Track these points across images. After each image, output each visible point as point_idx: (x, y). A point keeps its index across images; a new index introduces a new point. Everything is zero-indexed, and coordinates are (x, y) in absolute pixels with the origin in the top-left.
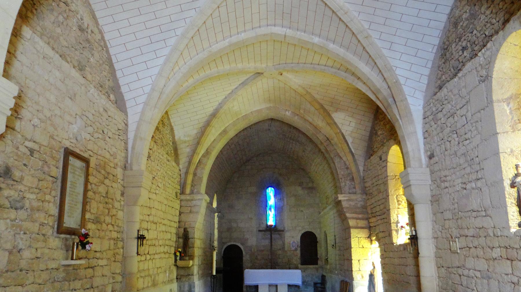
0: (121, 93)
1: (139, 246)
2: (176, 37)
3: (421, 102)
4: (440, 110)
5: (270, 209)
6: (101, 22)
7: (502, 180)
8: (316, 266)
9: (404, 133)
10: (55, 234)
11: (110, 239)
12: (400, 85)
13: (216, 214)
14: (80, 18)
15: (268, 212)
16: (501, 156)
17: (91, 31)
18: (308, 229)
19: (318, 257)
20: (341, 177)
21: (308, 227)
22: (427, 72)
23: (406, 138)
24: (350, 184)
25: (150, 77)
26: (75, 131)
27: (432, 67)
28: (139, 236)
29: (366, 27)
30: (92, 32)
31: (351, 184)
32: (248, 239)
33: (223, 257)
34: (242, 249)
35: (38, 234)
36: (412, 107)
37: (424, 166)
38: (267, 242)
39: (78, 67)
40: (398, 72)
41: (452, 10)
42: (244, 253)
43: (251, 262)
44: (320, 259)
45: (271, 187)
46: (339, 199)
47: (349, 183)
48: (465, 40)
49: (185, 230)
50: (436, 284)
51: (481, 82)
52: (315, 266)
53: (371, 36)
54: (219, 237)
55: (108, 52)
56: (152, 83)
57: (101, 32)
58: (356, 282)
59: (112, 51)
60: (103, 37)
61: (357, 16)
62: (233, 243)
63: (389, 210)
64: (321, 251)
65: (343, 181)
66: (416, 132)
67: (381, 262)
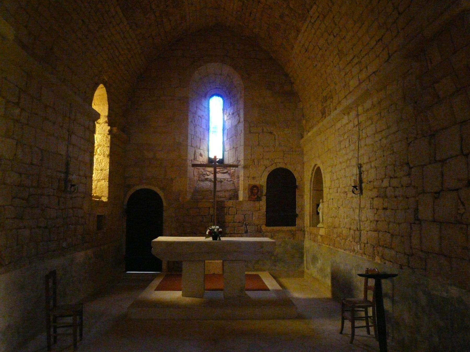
8: (293, 228)
21: (281, 161)
34: (163, 197)
42: (165, 204)
45: (218, 95)
52: (289, 228)
67: (260, 237)
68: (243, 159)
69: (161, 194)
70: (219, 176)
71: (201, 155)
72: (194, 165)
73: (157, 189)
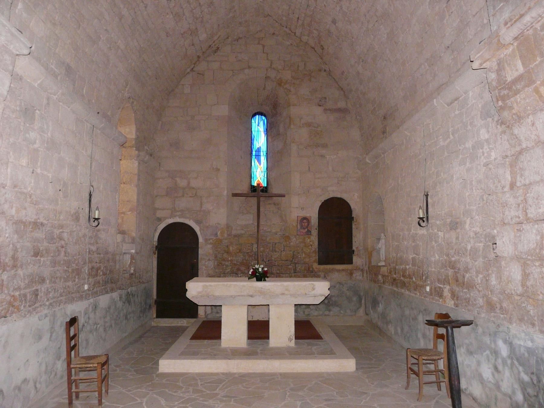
5: (258, 156)
15: (254, 162)
18: (334, 192)
19: (354, 248)
32: (209, 212)
38: (249, 219)
42: (201, 240)
43: (216, 257)
44: (356, 253)
62: (178, 220)
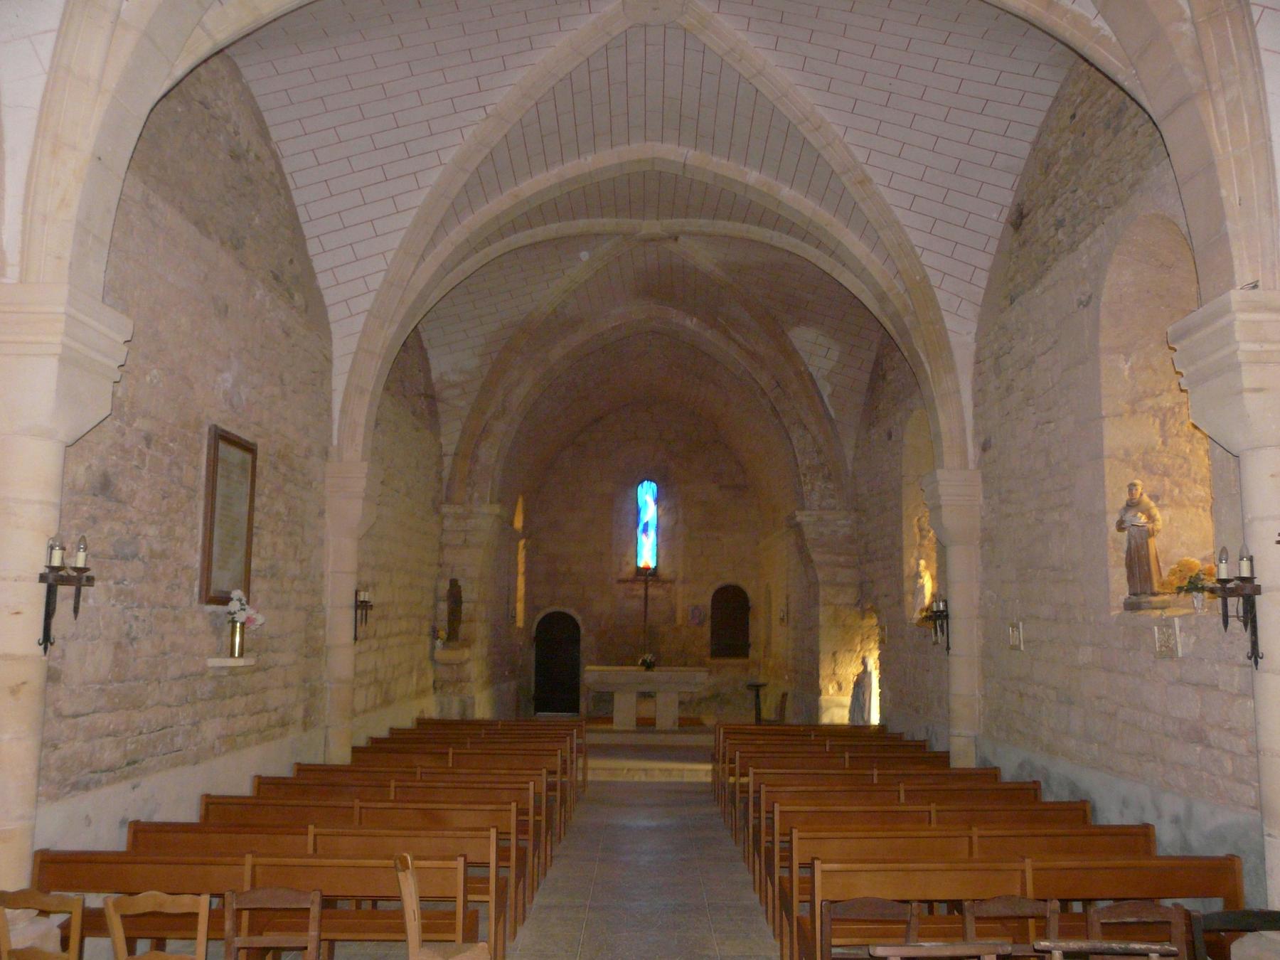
0: (318, 290)
1: (359, 624)
2: (441, 168)
3: (973, 327)
4: (1008, 351)
5: (645, 530)
6: (275, 134)
7: (1104, 513)
8: (745, 661)
9: (935, 394)
10: (196, 604)
11: (298, 609)
12: (930, 287)
13: (522, 543)
14: (232, 130)
15: (642, 539)
16: (1107, 463)
17: (256, 156)
18: (729, 578)
20: (804, 472)
22: (985, 261)
23: (937, 402)
24: (823, 486)
25: (381, 256)
26: (228, 385)
27: (998, 251)
28: (359, 603)
29: (860, 155)
30: (258, 158)
31: (825, 487)
33: (536, 639)
35: (164, 606)
36: (953, 339)
37: (971, 466)
39: (229, 243)
40: (926, 259)
41: (1040, 135)
42: (583, 631)
46: (798, 519)
47: (820, 486)
48: (1060, 205)
49: (454, 583)
50: (979, 710)
51: (1081, 306)
53: (870, 180)
54: (527, 594)
55: (289, 198)
56: (386, 268)
57: (275, 156)
58: (826, 697)
59: (298, 197)
60: (279, 167)
61: (841, 134)
63: (900, 549)
64: (757, 629)
65: (807, 481)
66: (958, 391)
68: (1026, 157)
69: (579, 618)
70: (652, 591)
71: (628, 563)
72: (620, 581)
73: (572, 612)
